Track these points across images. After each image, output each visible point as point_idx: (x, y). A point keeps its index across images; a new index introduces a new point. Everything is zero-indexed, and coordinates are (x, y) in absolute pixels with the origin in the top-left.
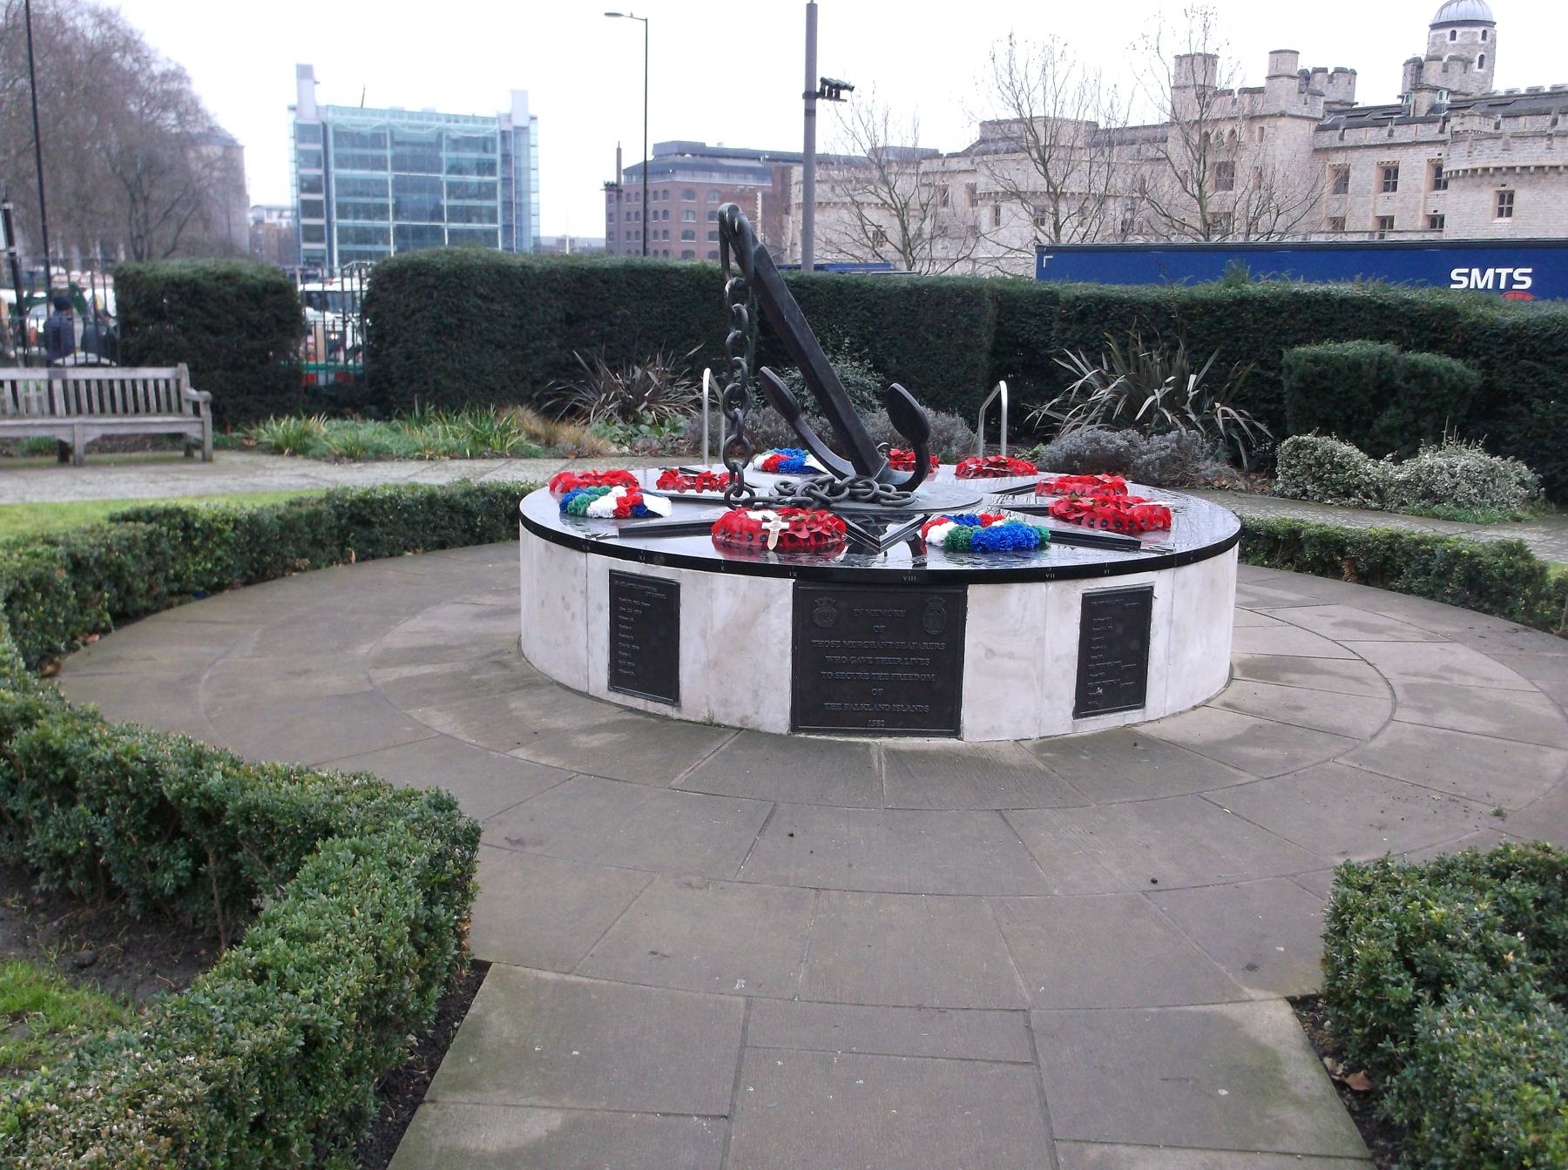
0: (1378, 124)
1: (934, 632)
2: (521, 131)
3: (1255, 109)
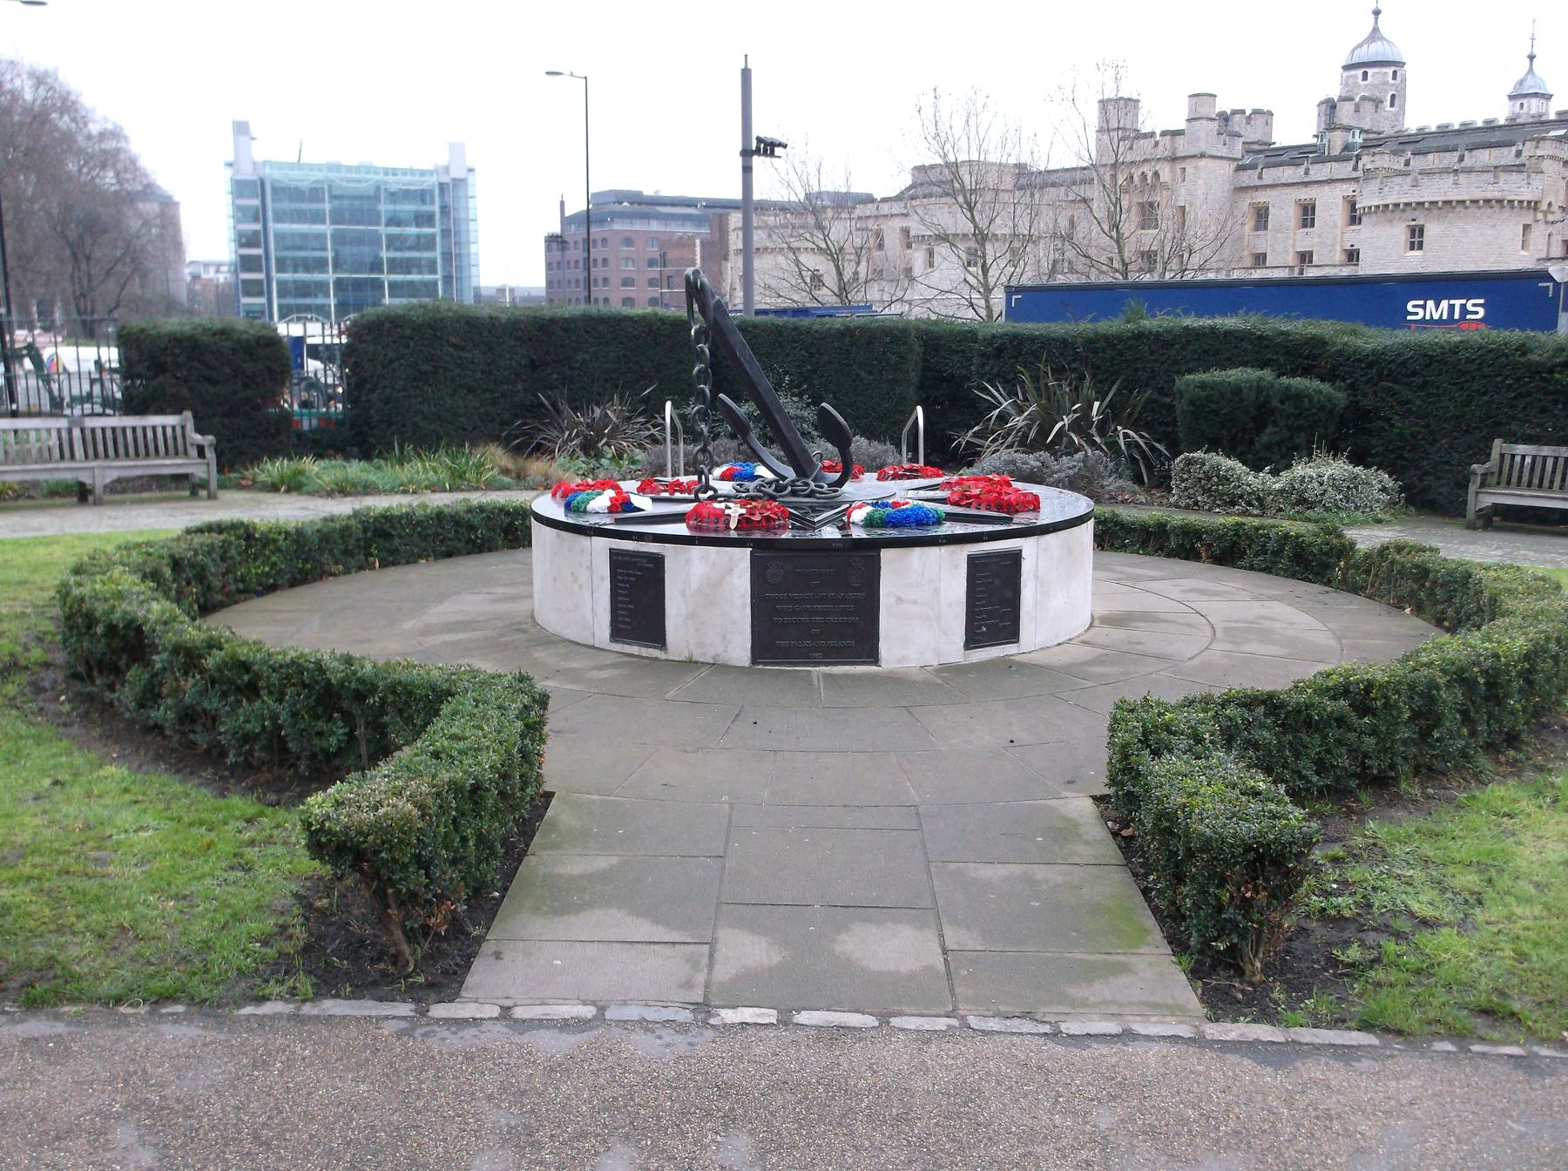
0: (1294, 163)
2: (459, 183)
3: (1176, 152)
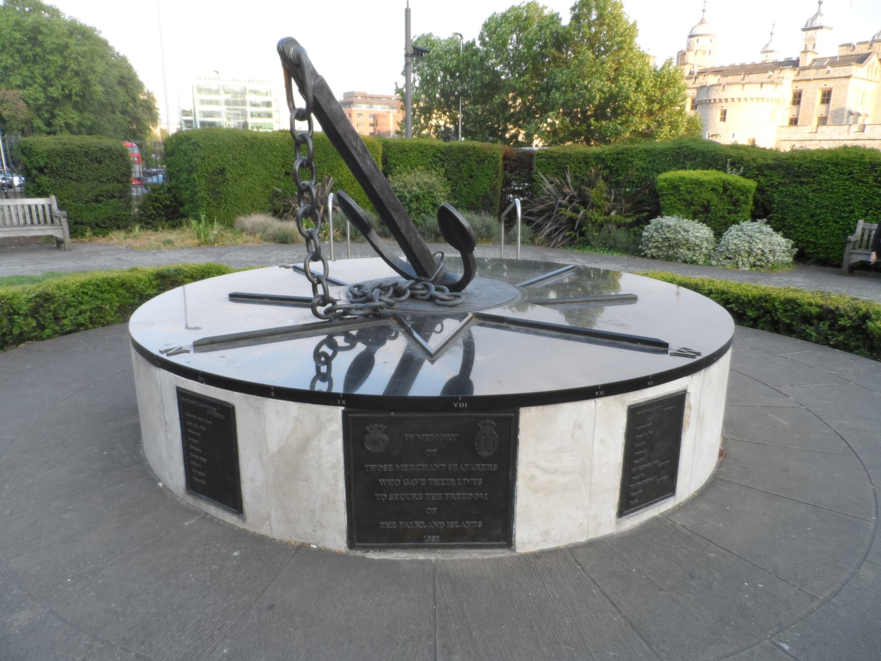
1: (485, 454)
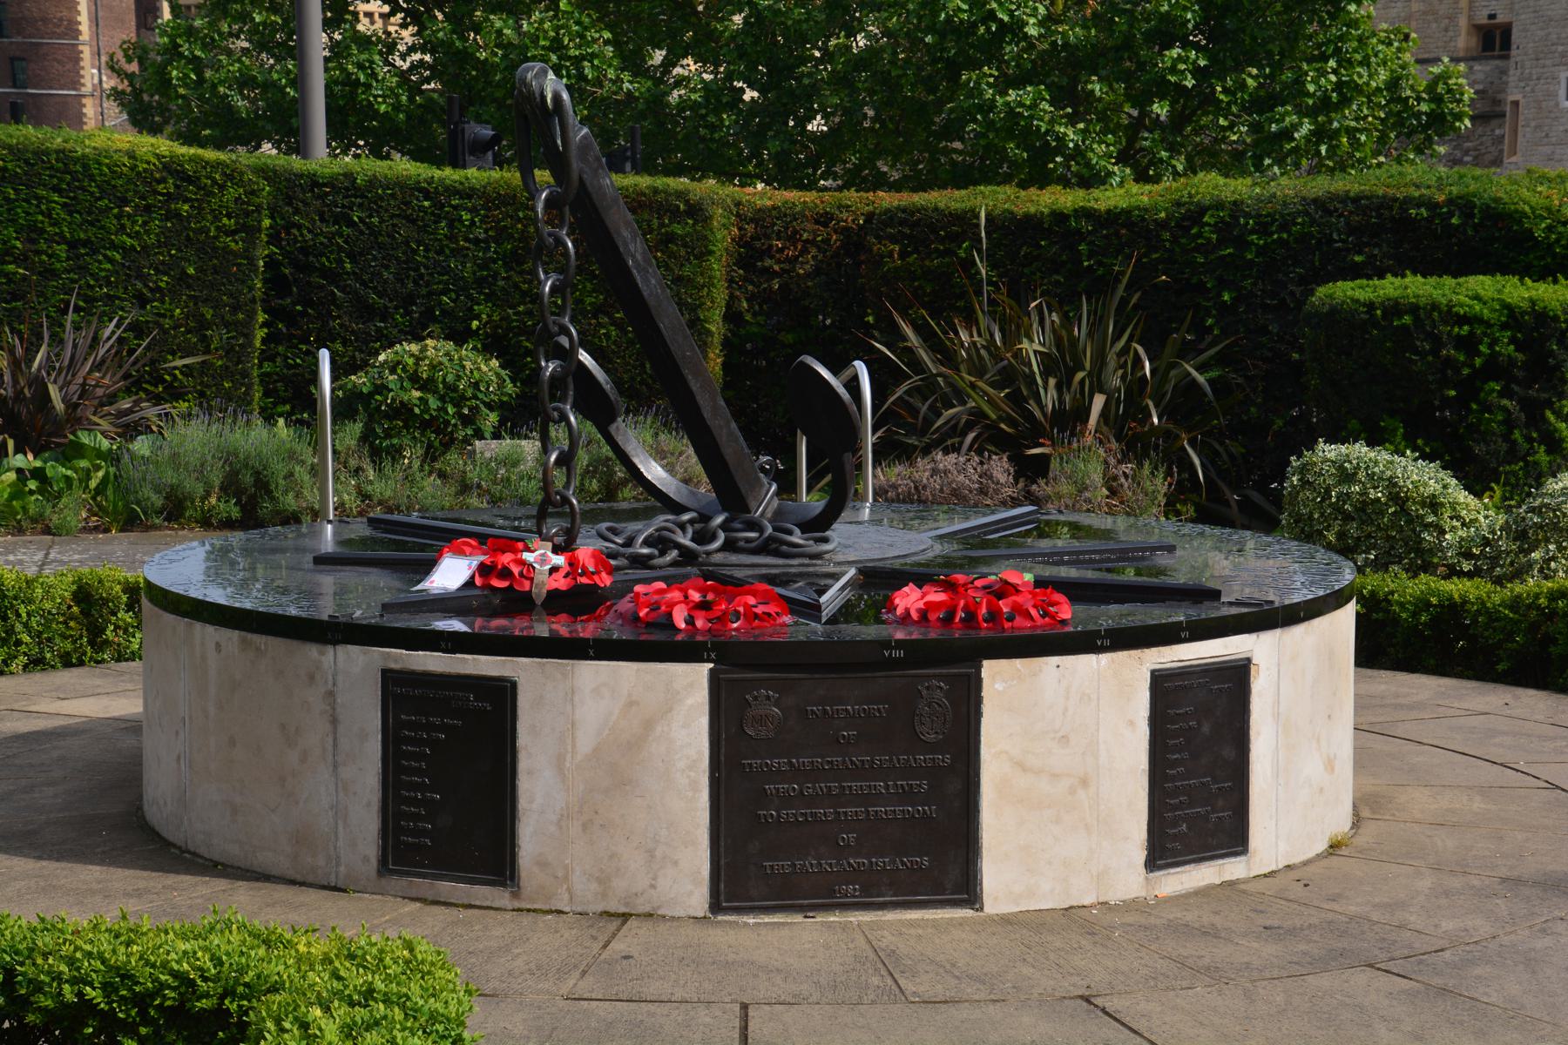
1: (931, 737)
